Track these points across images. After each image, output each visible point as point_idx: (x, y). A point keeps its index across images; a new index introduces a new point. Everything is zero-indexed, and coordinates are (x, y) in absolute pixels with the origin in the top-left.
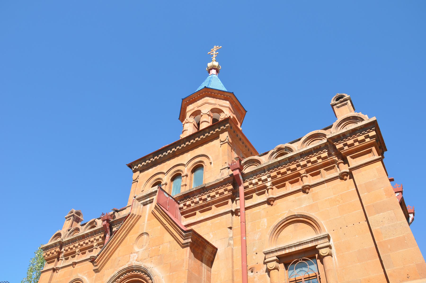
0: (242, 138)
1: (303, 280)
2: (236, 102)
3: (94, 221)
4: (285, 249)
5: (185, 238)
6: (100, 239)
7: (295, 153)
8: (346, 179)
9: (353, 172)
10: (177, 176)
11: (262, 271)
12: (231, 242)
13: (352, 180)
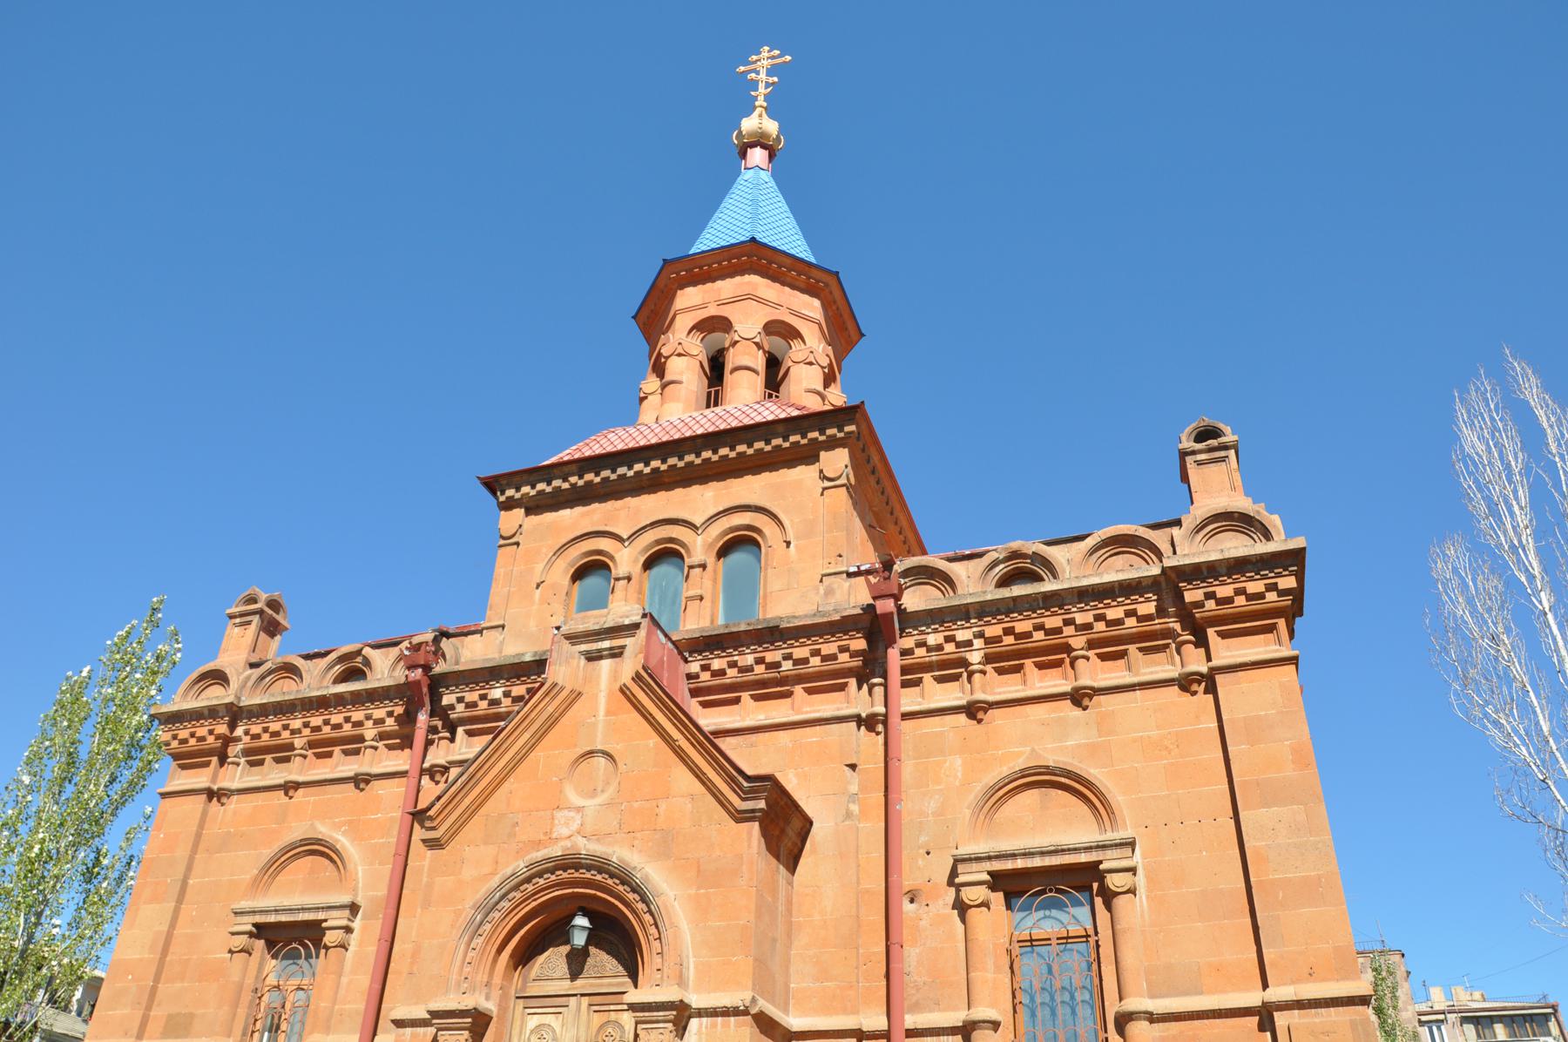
0: (879, 466)
1: (1054, 942)
2: (840, 302)
3: (359, 652)
4: (1013, 856)
5: (746, 795)
6: (390, 721)
7: (1066, 586)
9: (1219, 679)
10: (682, 565)
11: (941, 902)
12: (855, 808)
13: (1210, 697)
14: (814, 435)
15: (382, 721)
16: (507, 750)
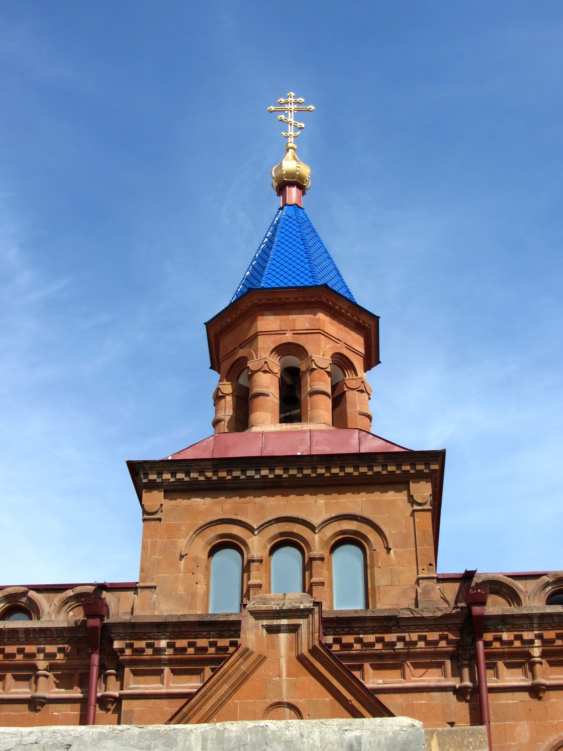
8: (108, 710)
14: (407, 468)
15: (53, 656)
16: (210, 697)
